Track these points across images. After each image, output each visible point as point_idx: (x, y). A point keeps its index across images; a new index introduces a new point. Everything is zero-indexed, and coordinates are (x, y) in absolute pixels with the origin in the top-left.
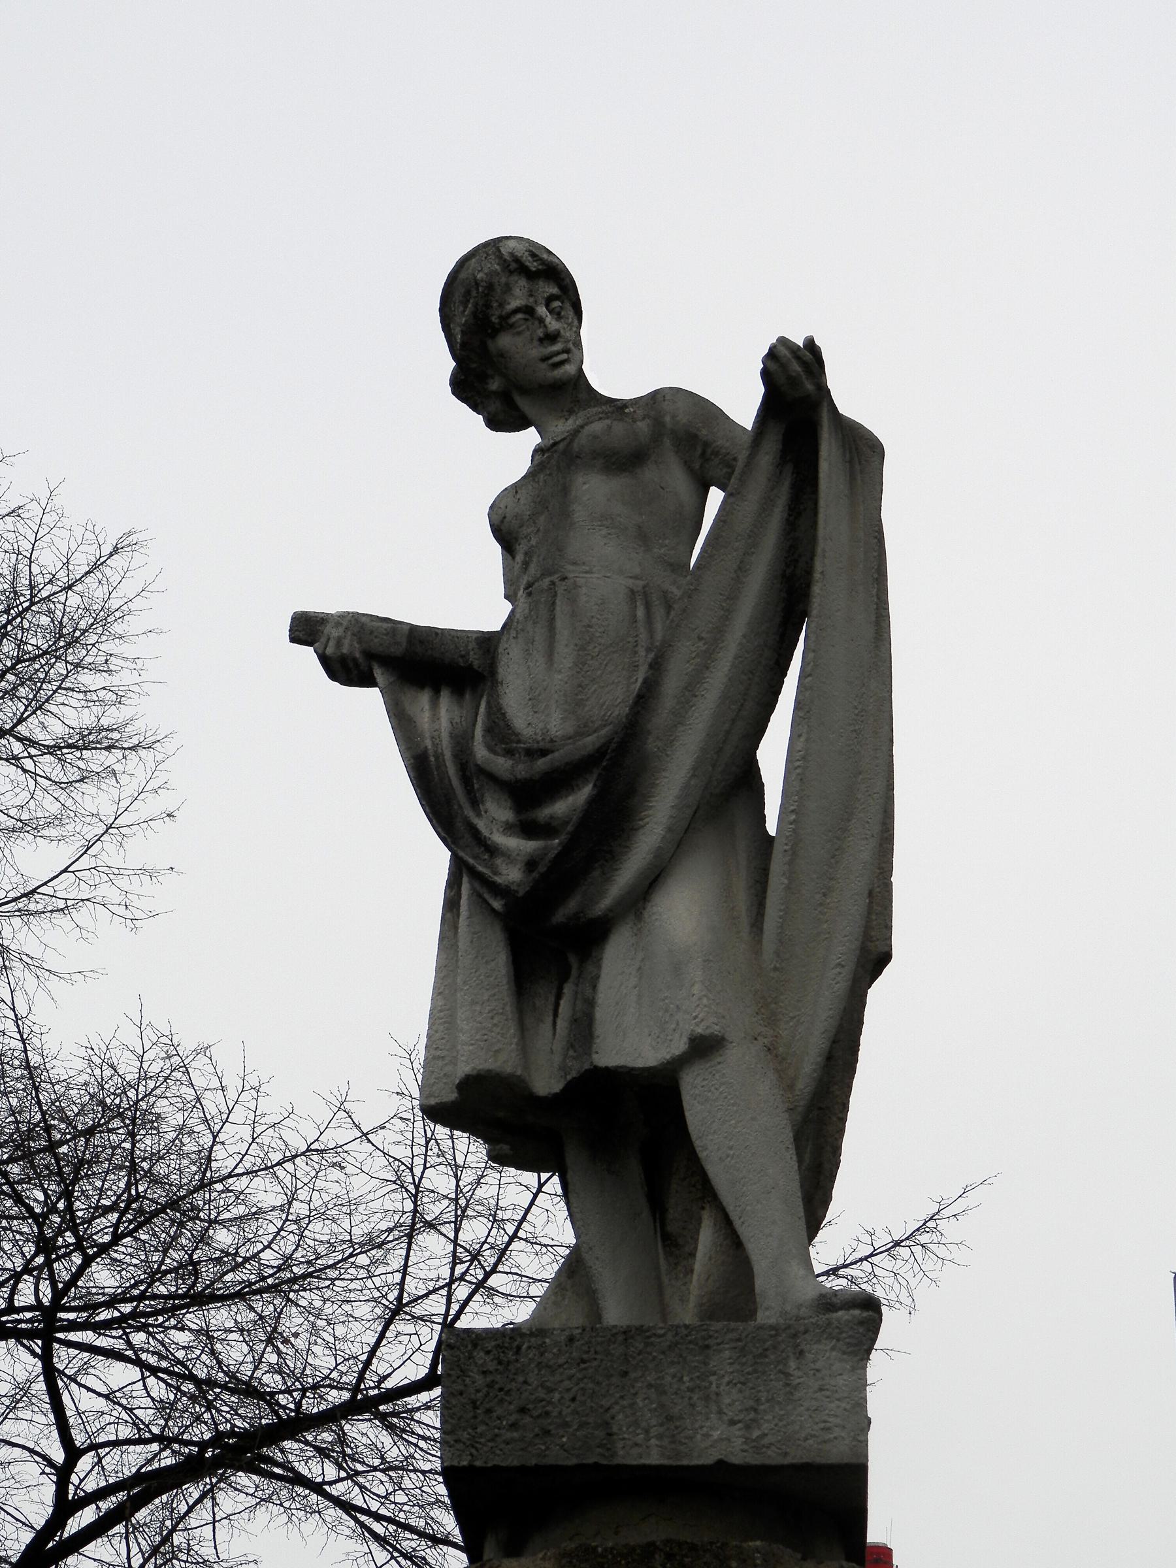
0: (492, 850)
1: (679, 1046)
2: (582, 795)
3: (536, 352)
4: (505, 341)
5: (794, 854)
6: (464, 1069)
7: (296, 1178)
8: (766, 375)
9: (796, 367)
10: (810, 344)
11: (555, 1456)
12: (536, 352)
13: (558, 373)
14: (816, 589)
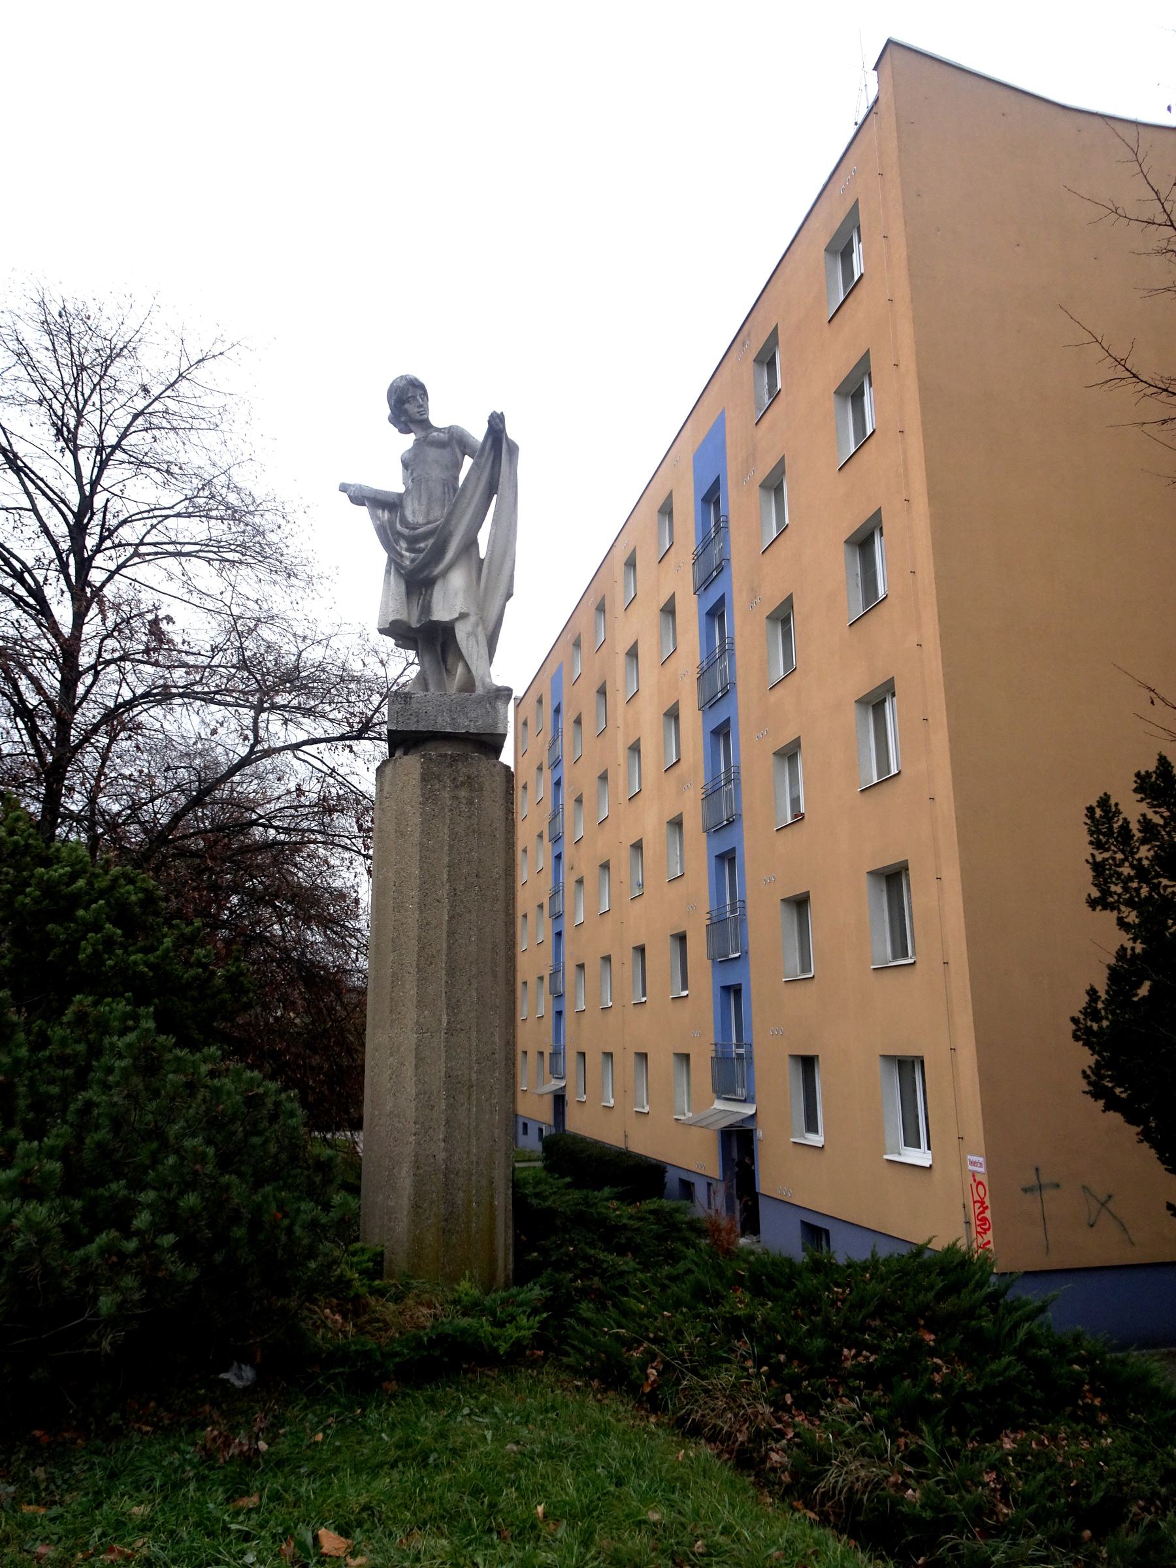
0: (402, 556)
1: (456, 615)
2: (431, 541)
3: (416, 410)
4: (407, 406)
5: (490, 563)
6: (391, 618)
7: (142, 543)
8: (489, 422)
9: (498, 421)
10: (502, 413)
11: (421, 728)
12: (416, 410)
13: (422, 417)
14: (500, 487)
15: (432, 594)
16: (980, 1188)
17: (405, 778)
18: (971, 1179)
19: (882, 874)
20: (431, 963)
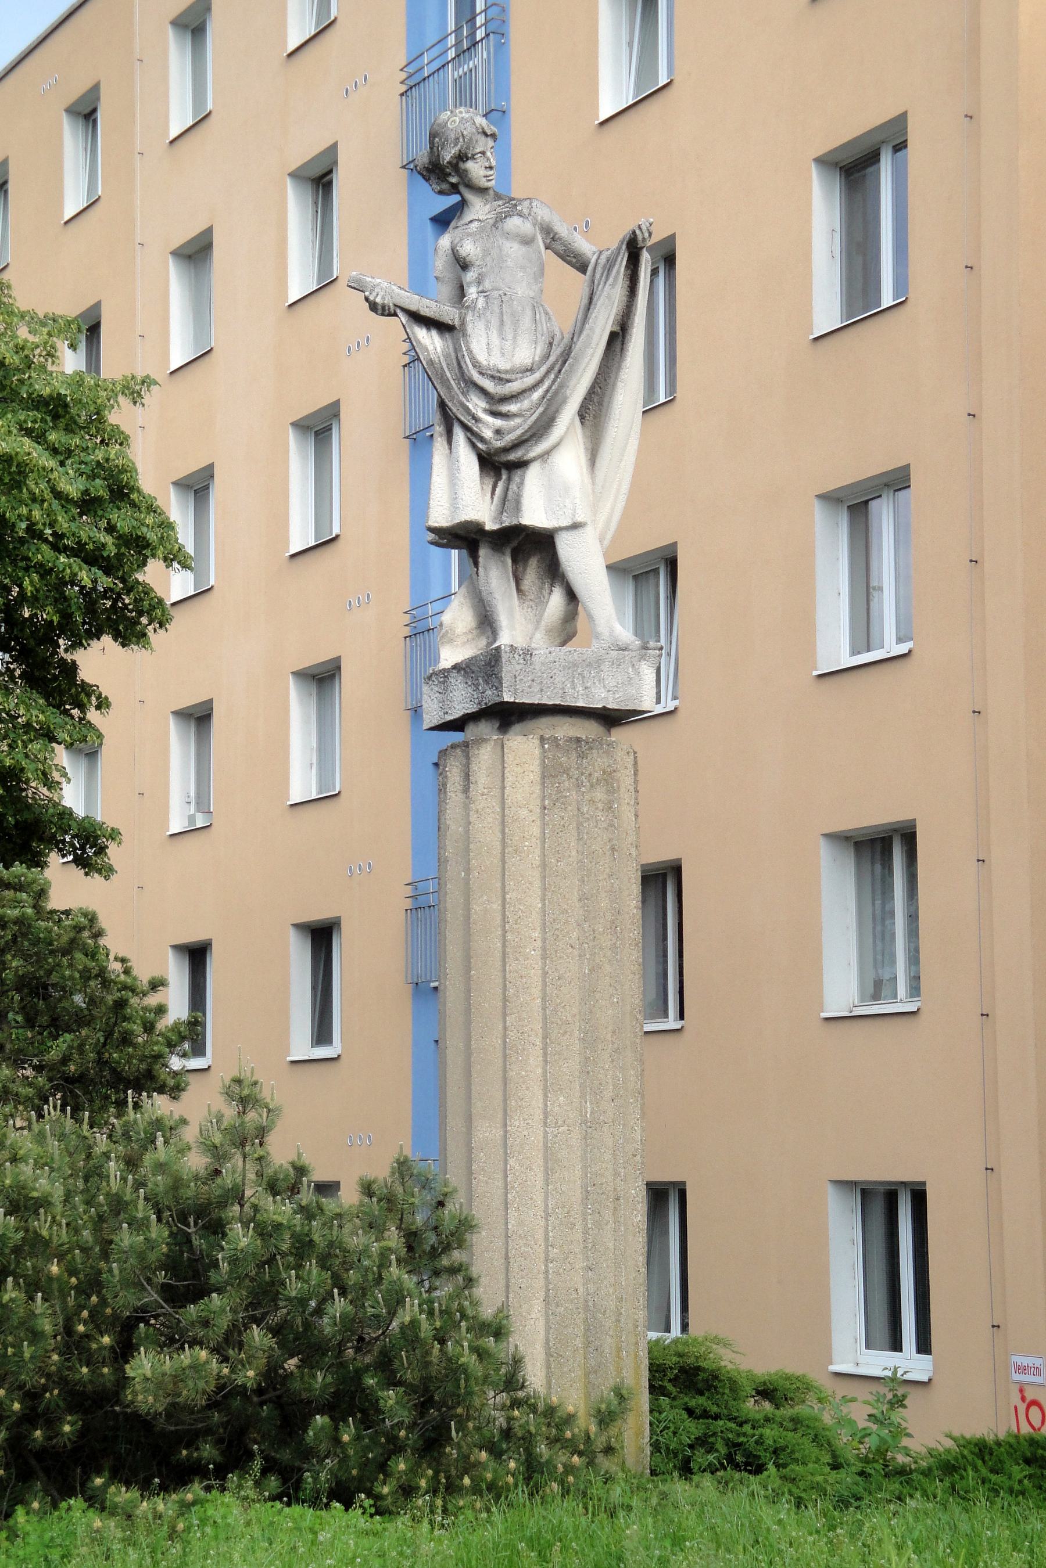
15: (522, 483)
16: (1035, 1412)
17: (519, 769)
18: (1016, 1399)
19: (314, 677)
20: (566, 1032)
